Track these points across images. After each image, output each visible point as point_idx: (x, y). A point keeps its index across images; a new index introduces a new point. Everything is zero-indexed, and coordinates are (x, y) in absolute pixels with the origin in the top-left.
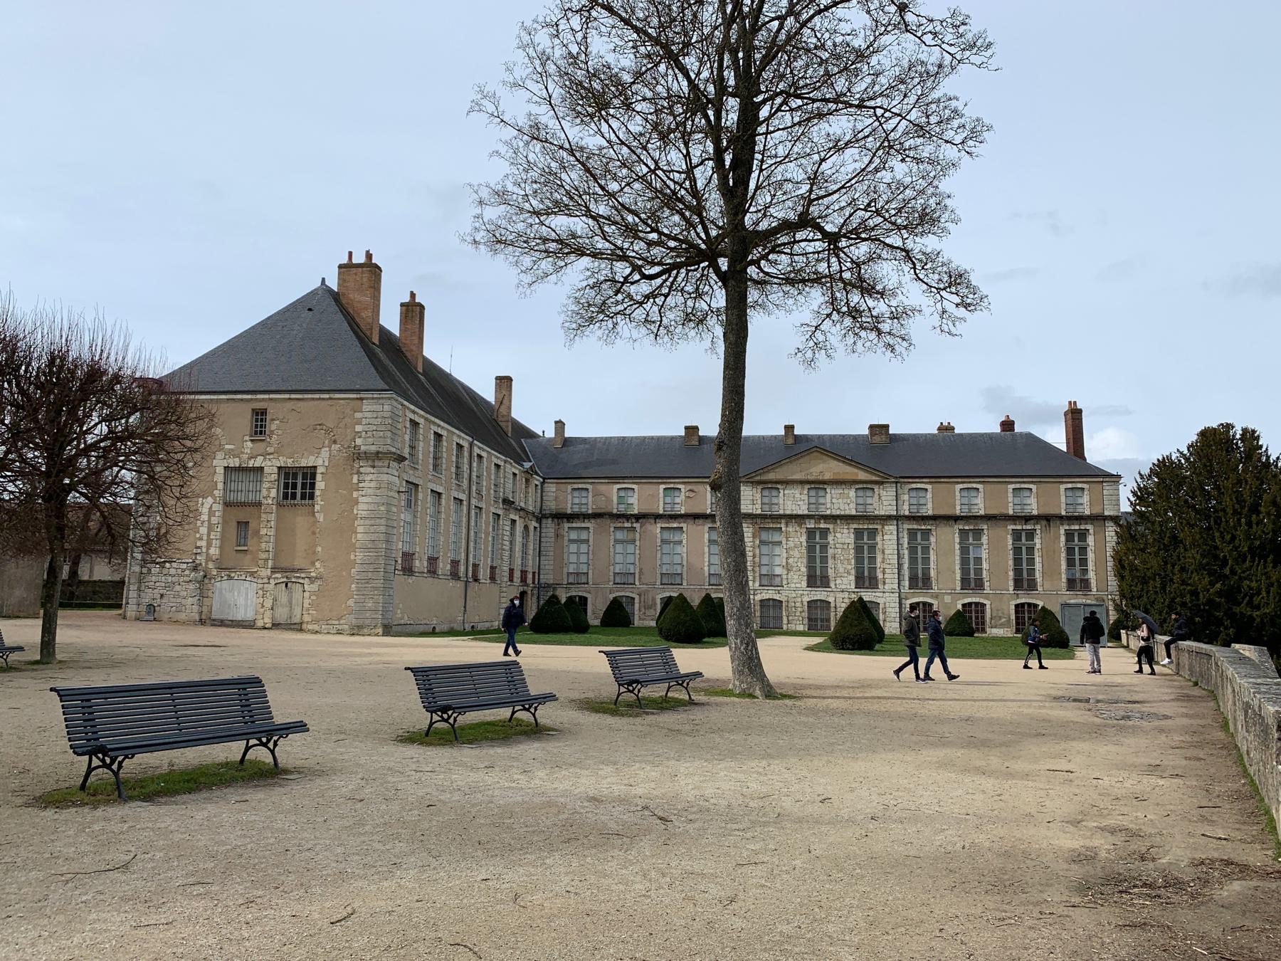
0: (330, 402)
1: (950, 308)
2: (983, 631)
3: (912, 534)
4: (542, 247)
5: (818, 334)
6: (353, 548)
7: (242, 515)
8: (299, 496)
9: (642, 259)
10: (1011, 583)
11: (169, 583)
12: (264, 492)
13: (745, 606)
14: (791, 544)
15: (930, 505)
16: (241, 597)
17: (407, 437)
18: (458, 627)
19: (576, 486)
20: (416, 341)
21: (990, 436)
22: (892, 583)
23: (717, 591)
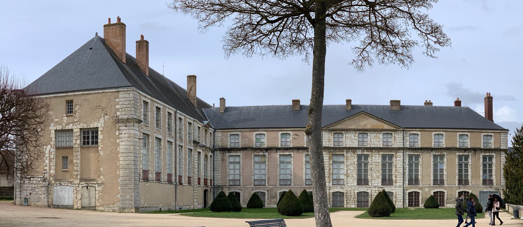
0: (103, 94)
1: (432, 43)
2: (443, 205)
3: (410, 157)
4: (212, 8)
5: (364, 53)
6: (118, 168)
7: (64, 153)
8: (90, 143)
9: (267, 12)
10: (457, 182)
11: (32, 188)
12: (74, 142)
13: (324, 196)
14: (349, 163)
15: (419, 143)
16: (66, 194)
17: (142, 110)
18: (173, 208)
19: (232, 133)
20: (145, 60)
21: (449, 108)
22: (400, 182)
23: (309, 188)
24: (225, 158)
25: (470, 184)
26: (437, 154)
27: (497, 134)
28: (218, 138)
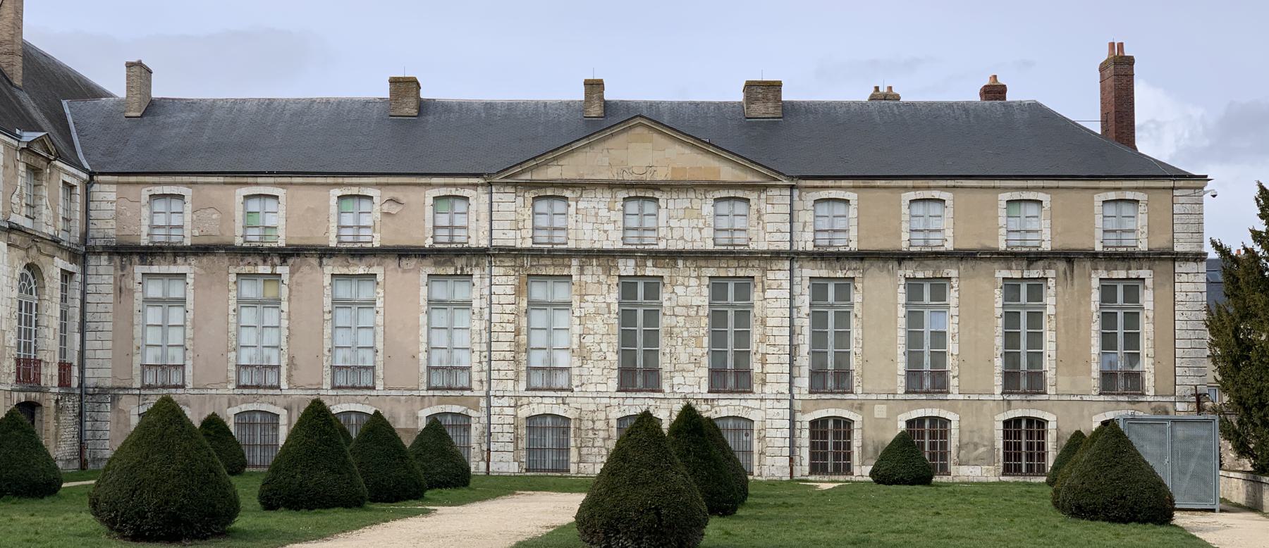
2: (945, 470)
3: (818, 287)
10: (998, 381)
14: (589, 308)
19: (158, 190)
21: (965, 108)
24: (129, 283)
25: (1051, 390)
26: (920, 275)
27: (1157, 194)
28: (104, 206)
